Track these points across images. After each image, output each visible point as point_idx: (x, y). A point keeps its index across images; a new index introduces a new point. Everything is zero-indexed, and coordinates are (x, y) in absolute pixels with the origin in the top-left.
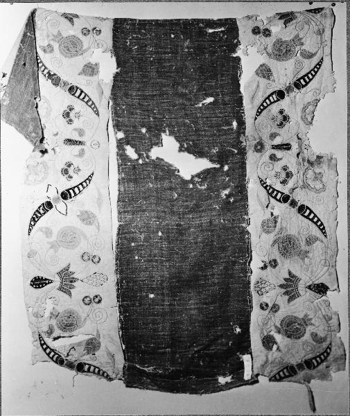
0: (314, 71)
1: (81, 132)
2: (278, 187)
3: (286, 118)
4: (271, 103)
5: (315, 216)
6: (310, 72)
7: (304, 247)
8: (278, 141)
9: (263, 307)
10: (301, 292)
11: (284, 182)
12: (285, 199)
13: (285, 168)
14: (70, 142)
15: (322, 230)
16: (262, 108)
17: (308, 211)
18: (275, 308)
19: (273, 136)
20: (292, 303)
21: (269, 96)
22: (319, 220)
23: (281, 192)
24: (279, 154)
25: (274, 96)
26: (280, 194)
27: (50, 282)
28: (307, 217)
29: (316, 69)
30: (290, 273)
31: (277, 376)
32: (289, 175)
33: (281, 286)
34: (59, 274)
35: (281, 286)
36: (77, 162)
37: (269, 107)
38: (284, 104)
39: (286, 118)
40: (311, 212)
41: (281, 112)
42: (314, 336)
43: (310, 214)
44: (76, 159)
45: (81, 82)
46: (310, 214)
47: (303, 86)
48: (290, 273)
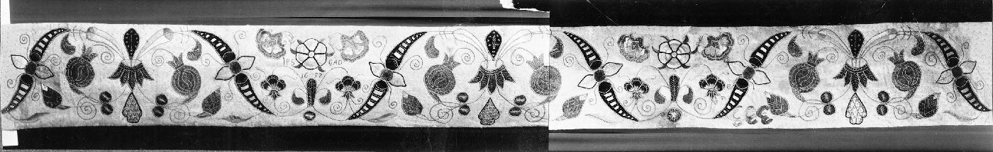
0: (580, 43)
1: (326, 100)
2: (726, 93)
3: (637, 82)
4: (615, 99)
5: (763, 45)
6: (581, 49)
7: (803, 58)
8: (666, 93)
9: (882, 110)
10: (862, 65)
11: (720, 86)
12: (742, 84)
13: (703, 84)
14: (312, 87)
15: (780, 38)
16: (621, 112)
17: (758, 54)
18: (884, 96)
19: (659, 99)
20: (876, 76)
21: (606, 101)
22: (768, 41)
23: (735, 89)
24: (683, 92)
25: (606, 96)
26: (737, 91)
27: (131, 54)
28: (765, 55)
29: (578, 41)
30: (839, 77)
31: (971, 101)
32: (712, 79)
33: (855, 88)
34: (141, 66)
35: (855, 88)
36: (286, 95)
37: (622, 104)
38: (617, 83)
39: (637, 82)
40: (759, 50)
41: (628, 87)
42: (916, 52)
43: (762, 52)
44: (290, 95)
45: (395, 94)
46: (762, 52)
47: (598, 57)
48: (839, 77)
